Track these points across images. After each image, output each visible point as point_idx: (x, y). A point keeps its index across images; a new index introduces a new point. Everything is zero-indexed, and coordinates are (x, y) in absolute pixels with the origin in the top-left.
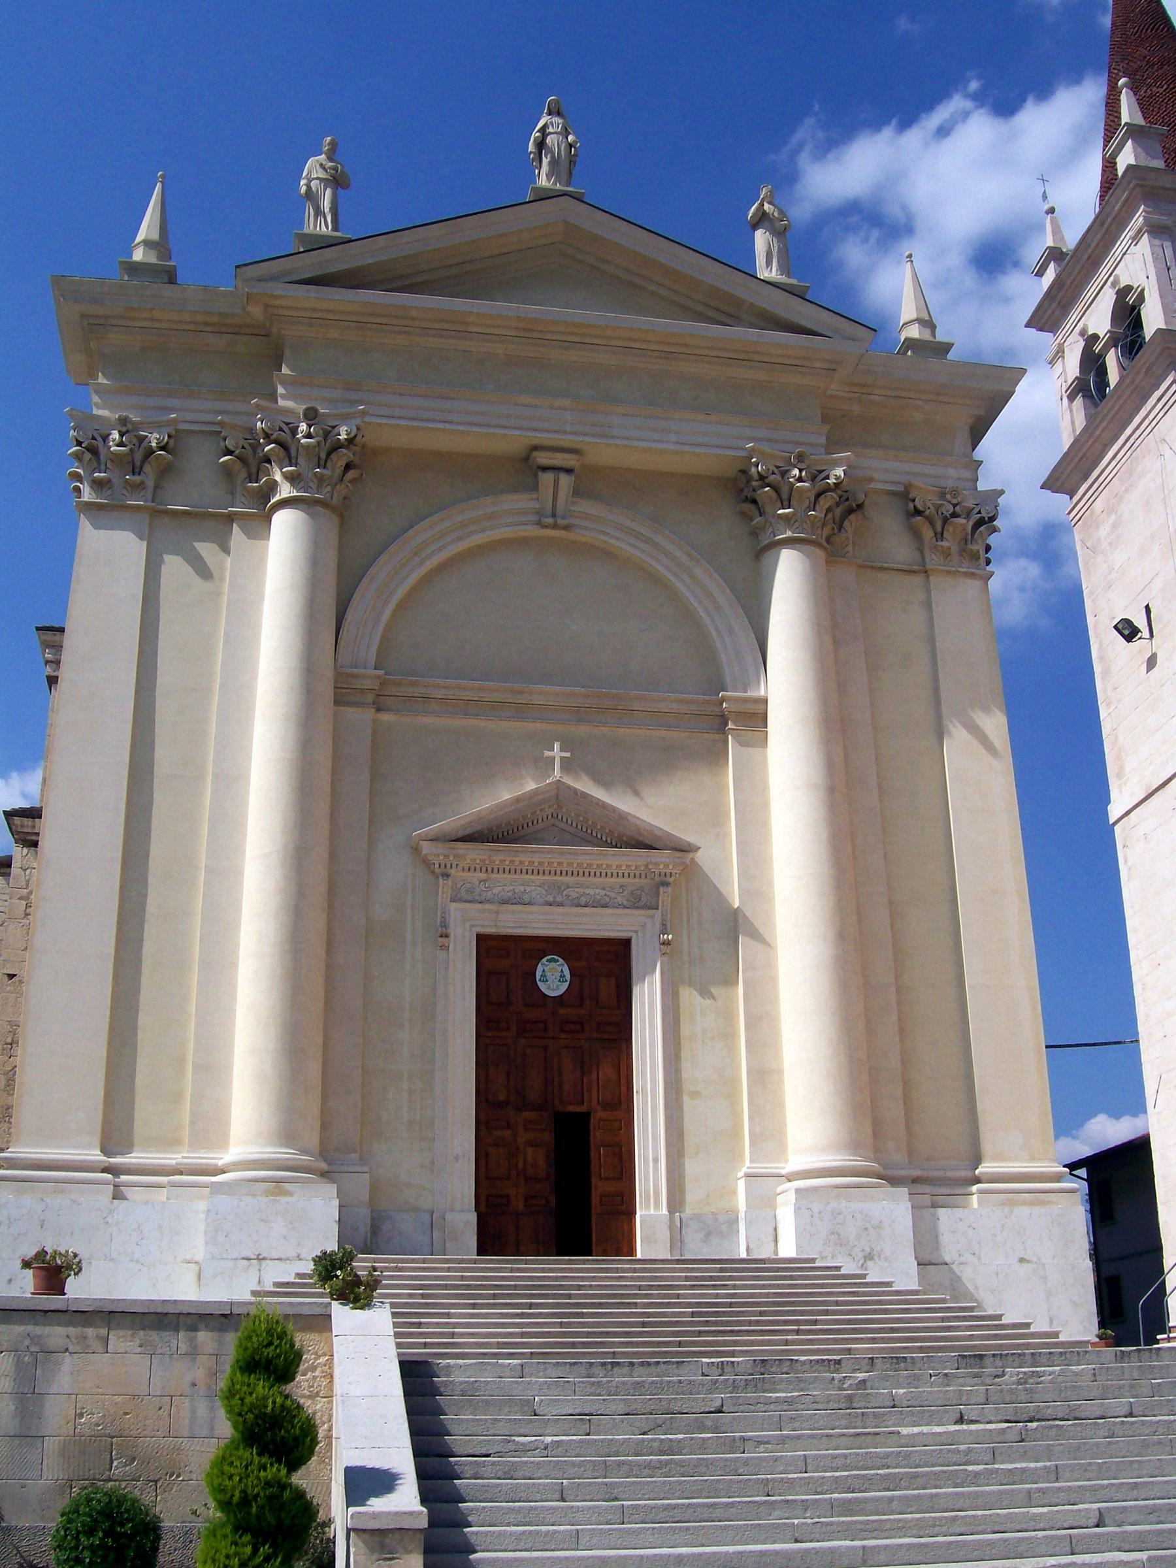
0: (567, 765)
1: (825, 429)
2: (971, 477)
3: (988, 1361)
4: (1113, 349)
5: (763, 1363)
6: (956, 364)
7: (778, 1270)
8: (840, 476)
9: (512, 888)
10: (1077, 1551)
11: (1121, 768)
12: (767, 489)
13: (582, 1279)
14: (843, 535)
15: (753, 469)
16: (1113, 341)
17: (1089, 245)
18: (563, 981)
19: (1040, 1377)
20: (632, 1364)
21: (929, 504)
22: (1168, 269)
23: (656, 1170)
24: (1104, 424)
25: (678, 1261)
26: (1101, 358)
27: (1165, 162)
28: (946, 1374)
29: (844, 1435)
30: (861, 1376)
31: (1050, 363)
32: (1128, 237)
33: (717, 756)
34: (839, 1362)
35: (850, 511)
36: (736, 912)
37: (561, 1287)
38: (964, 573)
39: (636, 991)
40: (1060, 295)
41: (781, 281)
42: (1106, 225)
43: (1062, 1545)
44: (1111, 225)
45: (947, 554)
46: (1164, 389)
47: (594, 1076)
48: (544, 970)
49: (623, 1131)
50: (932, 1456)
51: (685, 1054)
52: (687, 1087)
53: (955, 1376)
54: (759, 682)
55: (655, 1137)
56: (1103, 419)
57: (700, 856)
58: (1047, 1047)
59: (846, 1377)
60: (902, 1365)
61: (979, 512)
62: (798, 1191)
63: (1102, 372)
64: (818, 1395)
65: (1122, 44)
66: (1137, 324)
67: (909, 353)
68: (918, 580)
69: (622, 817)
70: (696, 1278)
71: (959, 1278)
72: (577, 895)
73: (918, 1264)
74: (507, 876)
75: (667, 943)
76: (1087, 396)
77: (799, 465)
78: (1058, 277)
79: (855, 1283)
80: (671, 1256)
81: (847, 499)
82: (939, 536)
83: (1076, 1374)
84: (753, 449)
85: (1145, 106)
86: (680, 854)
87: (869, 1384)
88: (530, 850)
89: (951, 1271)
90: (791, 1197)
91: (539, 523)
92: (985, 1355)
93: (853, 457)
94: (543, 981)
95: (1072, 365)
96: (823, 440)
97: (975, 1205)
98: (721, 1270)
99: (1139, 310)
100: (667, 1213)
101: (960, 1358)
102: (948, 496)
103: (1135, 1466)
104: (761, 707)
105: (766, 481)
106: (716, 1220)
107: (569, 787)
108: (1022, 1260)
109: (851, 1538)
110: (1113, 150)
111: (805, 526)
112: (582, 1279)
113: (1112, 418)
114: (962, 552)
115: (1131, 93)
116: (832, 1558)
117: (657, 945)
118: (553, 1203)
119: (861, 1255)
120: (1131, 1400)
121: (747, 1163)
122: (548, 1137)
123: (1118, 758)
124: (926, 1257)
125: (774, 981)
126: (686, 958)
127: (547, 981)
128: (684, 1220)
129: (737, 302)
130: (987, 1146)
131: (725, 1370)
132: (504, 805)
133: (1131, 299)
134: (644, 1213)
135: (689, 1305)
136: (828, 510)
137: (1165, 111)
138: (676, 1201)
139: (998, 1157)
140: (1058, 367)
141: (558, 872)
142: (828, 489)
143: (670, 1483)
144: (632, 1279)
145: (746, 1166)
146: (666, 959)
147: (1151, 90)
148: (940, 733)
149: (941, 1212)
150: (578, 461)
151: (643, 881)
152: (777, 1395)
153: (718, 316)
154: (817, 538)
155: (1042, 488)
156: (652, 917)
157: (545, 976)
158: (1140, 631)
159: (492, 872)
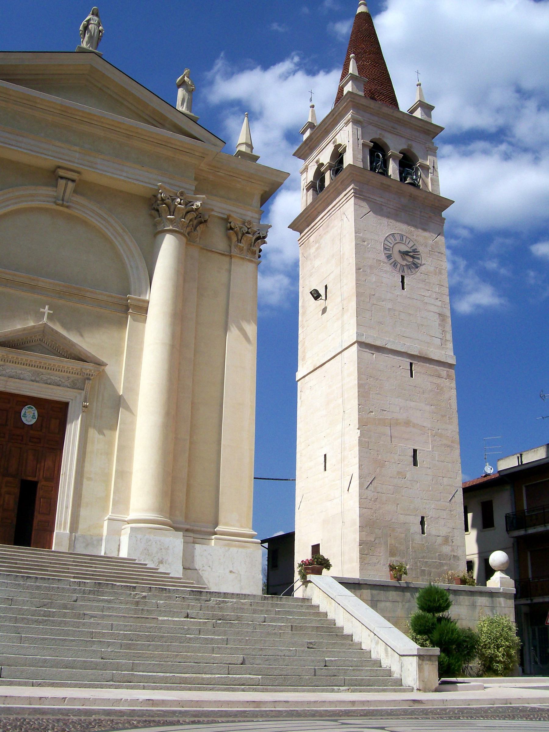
0: (50, 317)
1: (196, 183)
2: (258, 217)
3: (204, 594)
4: (329, 171)
5: (99, 584)
6: (260, 165)
7: (118, 562)
8: (199, 205)
9: (15, 371)
10: (230, 673)
11: (304, 357)
12: (165, 205)
13: (24, 556)
14: (195, 233)
15: (159, 195)
16: (330, 167)
17: (326, 123)
18: (34, 418)
19: (226, 603)
20: (37, 578)
21: (237, 226)
22: (358, 139)
23: (66, 512)
24: (320, 202)
25: (71, 554)
26: (323, 174)
27: (365, 94)
28: (183, 597)
29: (131, 617)
30: (144, 594)
31: (301, 173)
32: (343, 123)
33: (122, 324)
34: (135, 587)
35: (201, 223)
36: (120, 397)
37: (13, 559)
38: (248, 259)
39: (68, 427)
40: (310, 143)
41: (187, 113)
42: (335, 116)
43: (224, 670)
44: (337, 115)
45: (241, 249)
46: (348, 191)
47: (43, 464)
48: (25, 412)
49: (53, 492)
50: (171, 629)
51: (88, 456)
52: (86, 475)
53: (188, 599)
54: (146, 293)
55: (68, 496)
56: (320, 200)
57: (108, 369)
58: (254, 478)
59: (137, 594)
60: (164, 592)
61: (259, 233)
62: (131, 528)
63: (323, 180)
64: (122, 600)
65: (355, 41)
66: (341, 162)
67: (239, 157)
68: (227, 259)
69: (73, 345)
70: (78, 562)
71: (201, 577)
72: (46, 379)
73: (184, 568)
74: (14, 365)
75: (86, 407)
76: (315, 190)
77: (181, 197)
78: (311, 135)
79: (152, 572)
80: (68, 551)
81: (200, 217)
82: (239, 241)
83: (243, 604)
84: (161, 186)
85: (360, 69)
86: (98, 366)
87: (147, 598)
88: (26, 354)
89: (198, 573)
90: (128, 531)
91: (55, 203)
92: (203, 591)
93: (206, 198)
94: (24, 417)
95: (310, 176)
96: (194, 188)
97: (213, 545)
98: (91, 560)
99: (343, 156)
100: (69, 533)
101: (191, 591)
102: (246, 224)
103: (263, 642)
104: (146, 304)
105: (165, 202)
106: (92, 538)
107: (50, 327)
108: (231, 572)
109: (128, 659)
110: (343, 84)
111: (179, 225)
112: (24, 556)
113: (324, 201)
114: (249, 249)
115: (355, 62)
116: (118, 666)
117: (81, 406)
118: (15, 523)
119: (157, 561)
120: (265, 616)
121: (110, 514)
122: (17, 491)
123: (304, 352)
124: (187, 566)
125: (134, 430)
126: (94, 415)
127: (26, 417)
128: (77, 537)
129: (165, 118)
130: (222, 518)
131: (81, 586)
132: (18, 330)
133: (340, 150)
134: (58, 531)
135: (73, 573)
136: (191, 220)
137: (368, 73)
138: (74, 527)
139: (226, 524)
140: (304, 175)
141: (39, 367)
142: (192, 210)
143: (46, 629)
144: (48, 559)
145: (110, 515)
146: (84, 414)
147: (364, 63)
148: (226, 329)
149: (197, 546)
150: (78, 177)
151: (79, 376)
152: (104, 598)
153: (154, 123)
154: (184, 232)
155: (288, 227)
156: (80, 394)
157: (26, 415)
158: (321, 296)
159: (7, 362)
